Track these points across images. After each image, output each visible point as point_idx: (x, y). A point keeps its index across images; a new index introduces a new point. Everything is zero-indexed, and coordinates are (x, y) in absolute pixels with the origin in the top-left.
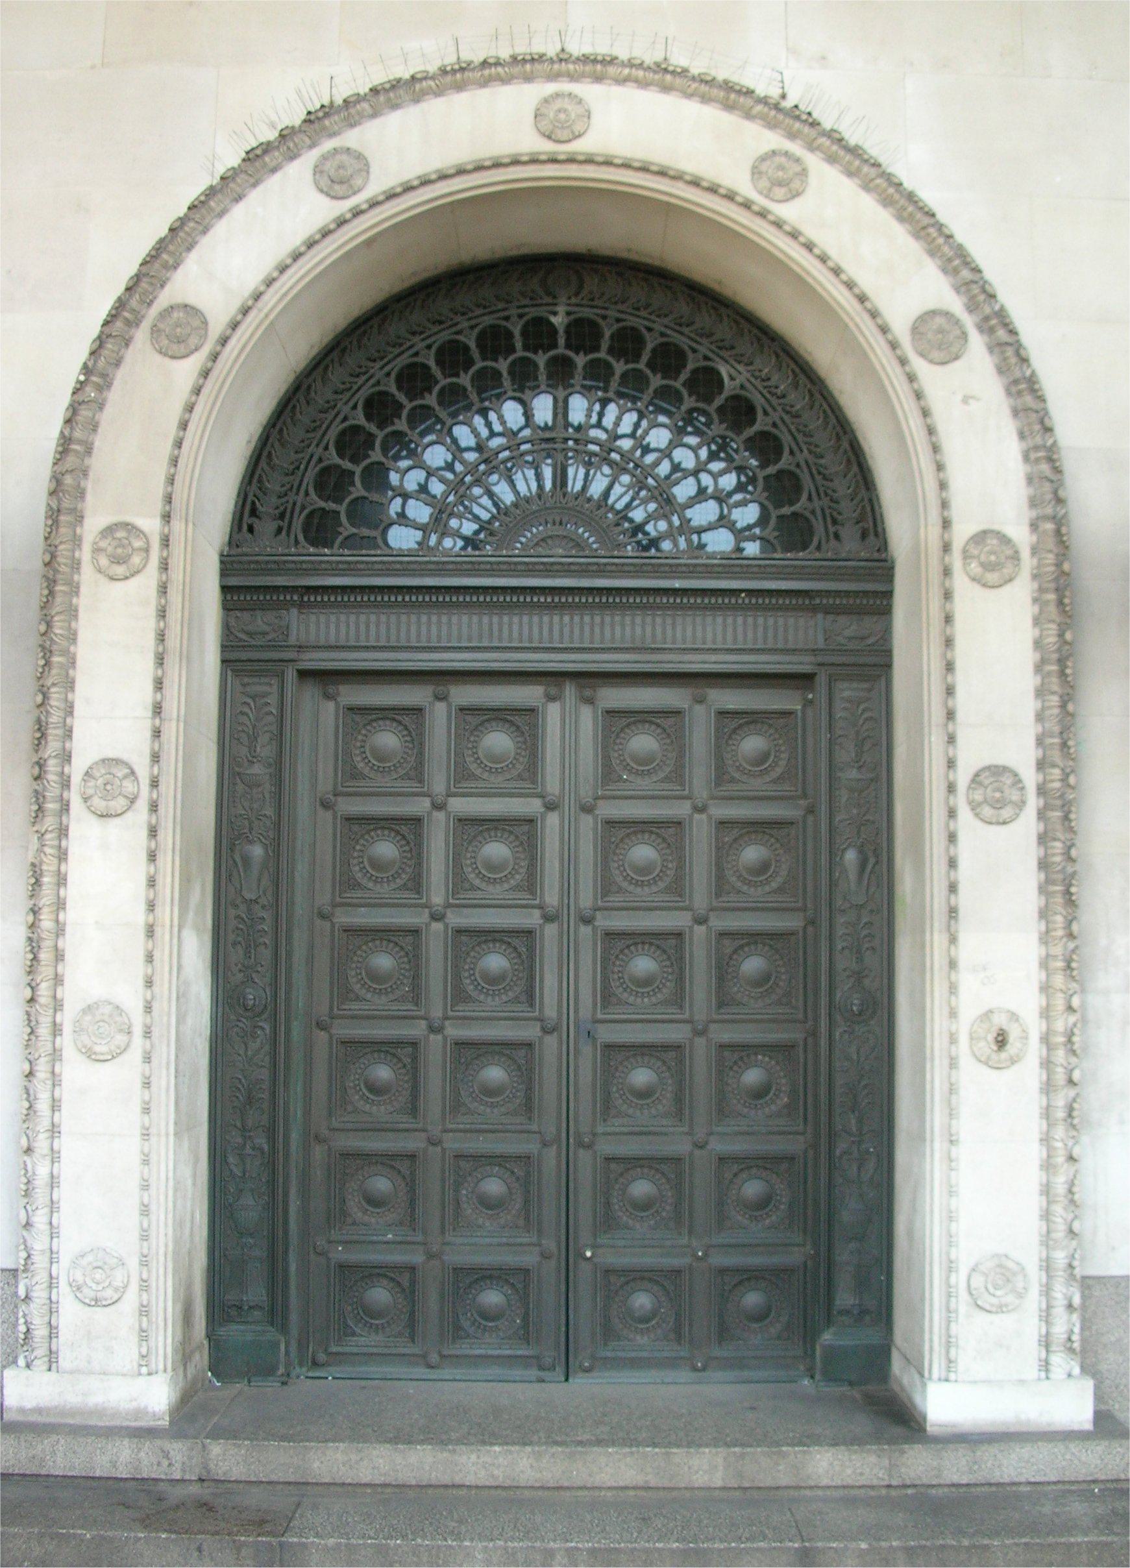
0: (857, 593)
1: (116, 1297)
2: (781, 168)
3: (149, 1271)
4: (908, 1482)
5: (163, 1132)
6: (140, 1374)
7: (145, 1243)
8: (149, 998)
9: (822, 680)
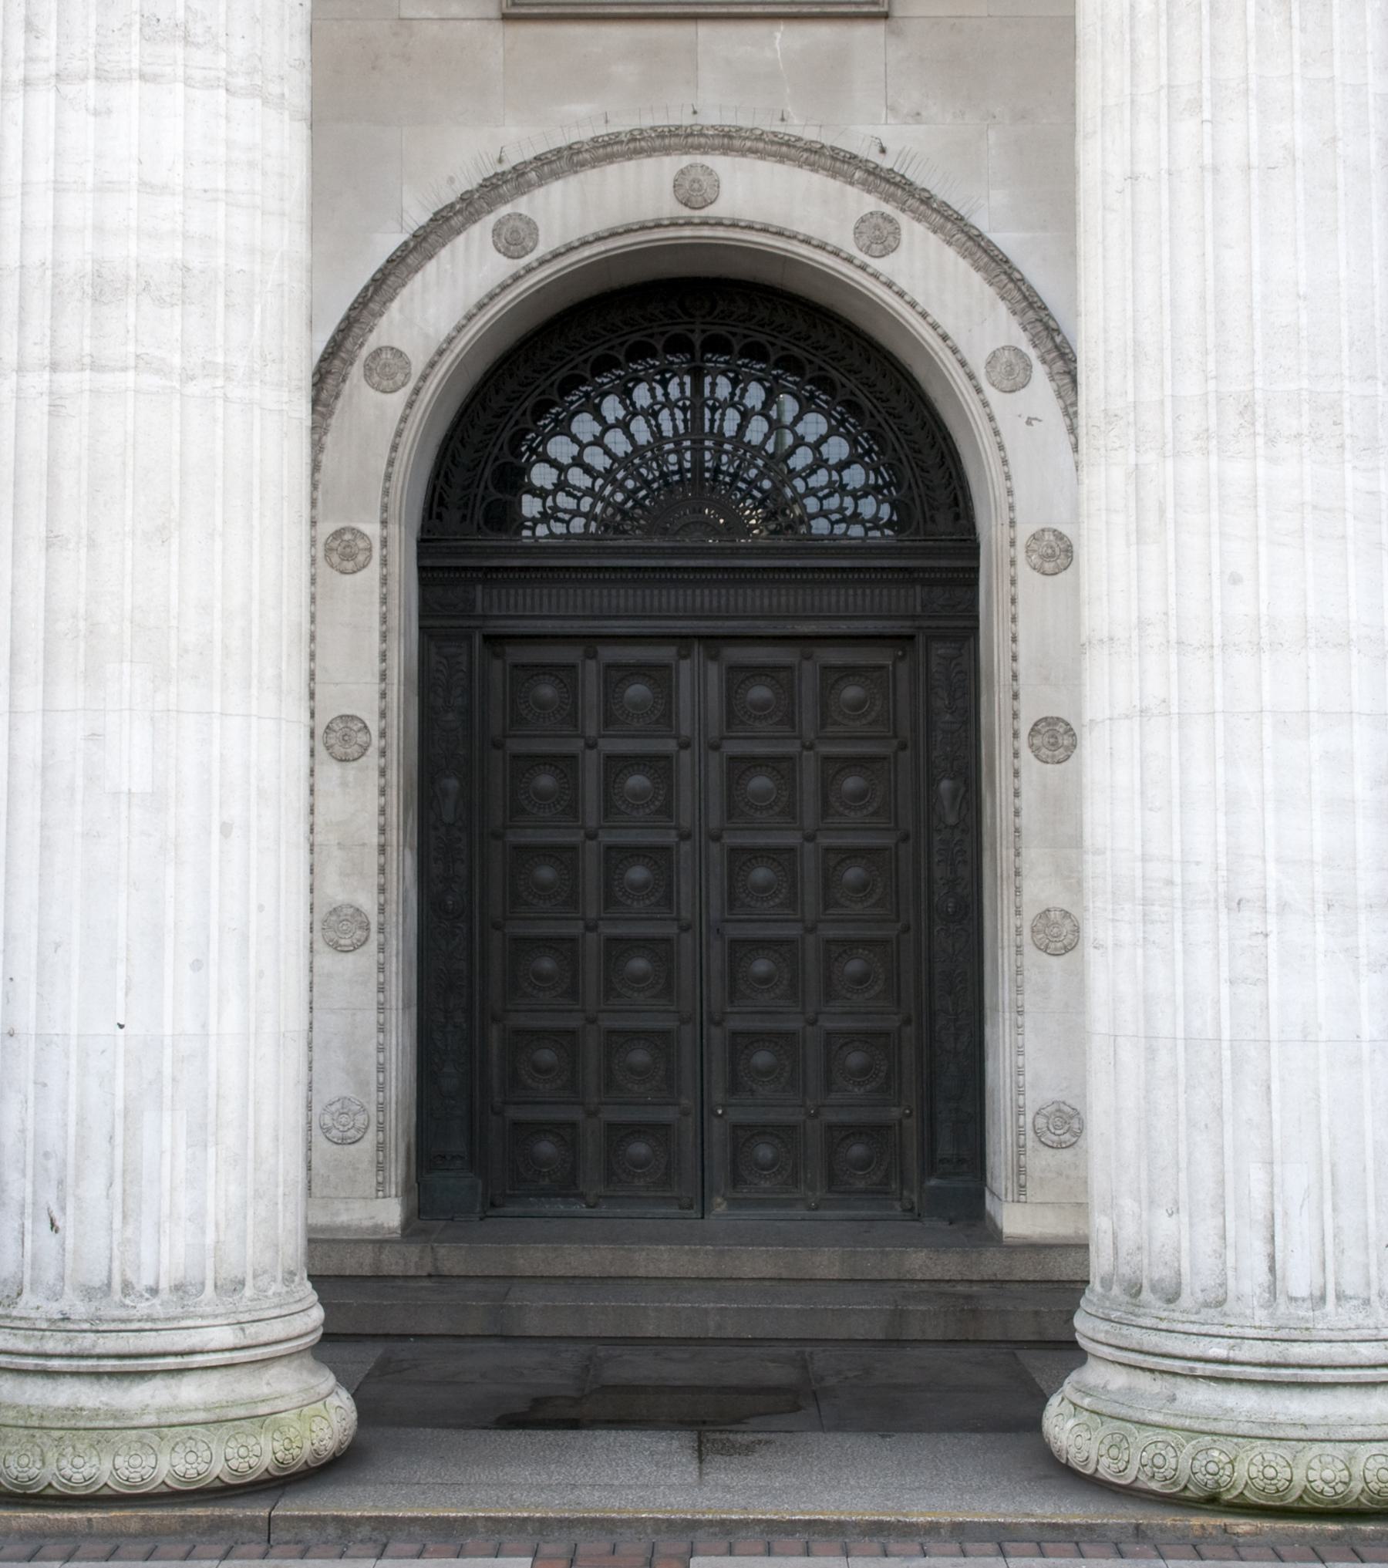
0: (947, 569)
1: (359, 1136)
2: (877, 227)
3: (384, 1116)
4: (986, 1278)
5: (394, 1007)
6: (377, 1197)
7: (381, 1094)
8: (382, 901)
9: (921, 640)
